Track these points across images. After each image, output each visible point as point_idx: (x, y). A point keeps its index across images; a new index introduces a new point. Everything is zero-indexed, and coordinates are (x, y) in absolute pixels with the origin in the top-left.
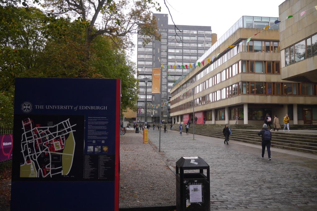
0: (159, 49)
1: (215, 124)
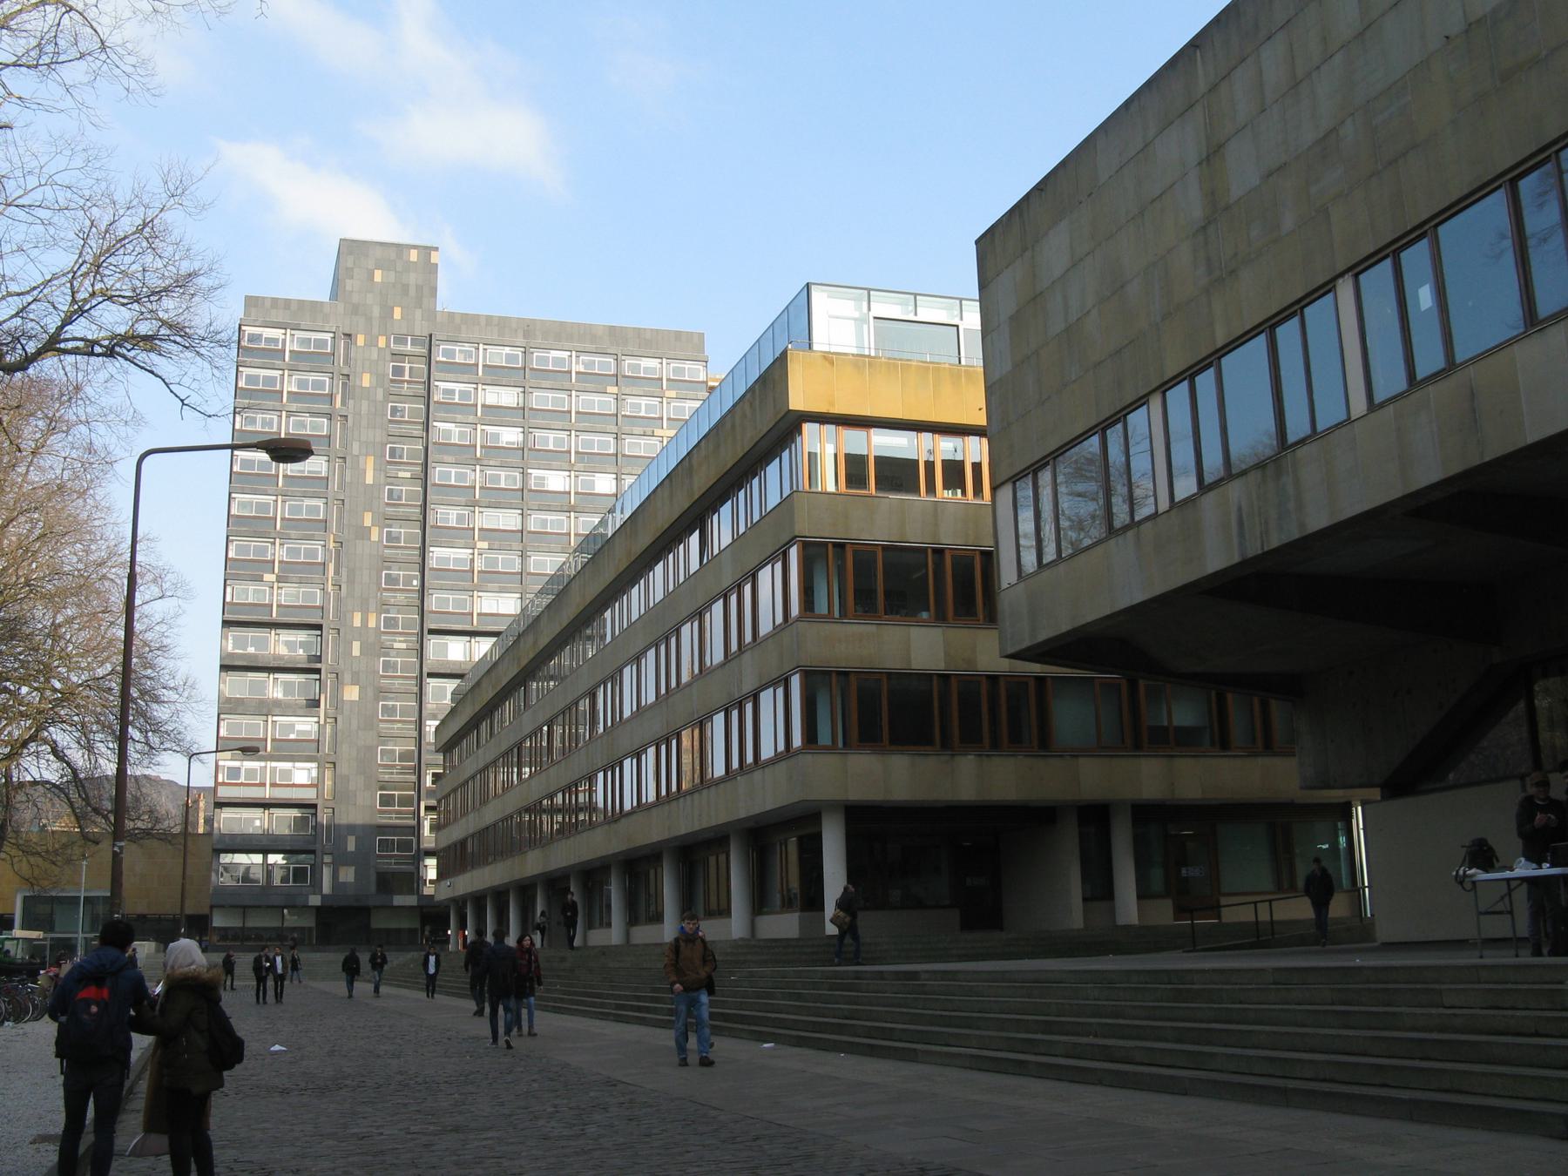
0: (370, 461)
1: (1257, 921)
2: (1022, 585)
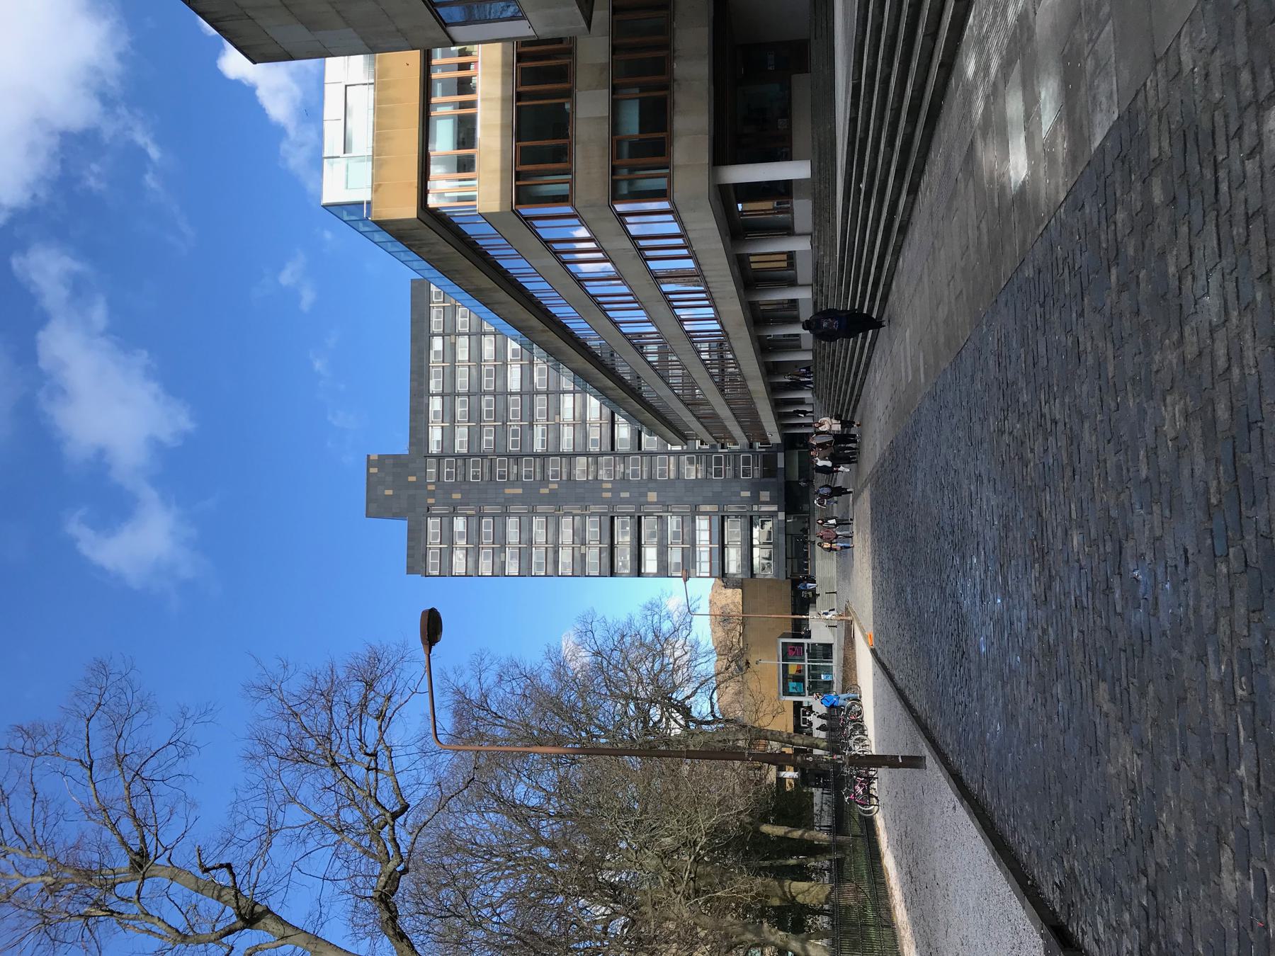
0: (508, 491)
1: (812, 350)
2: (529, 15)
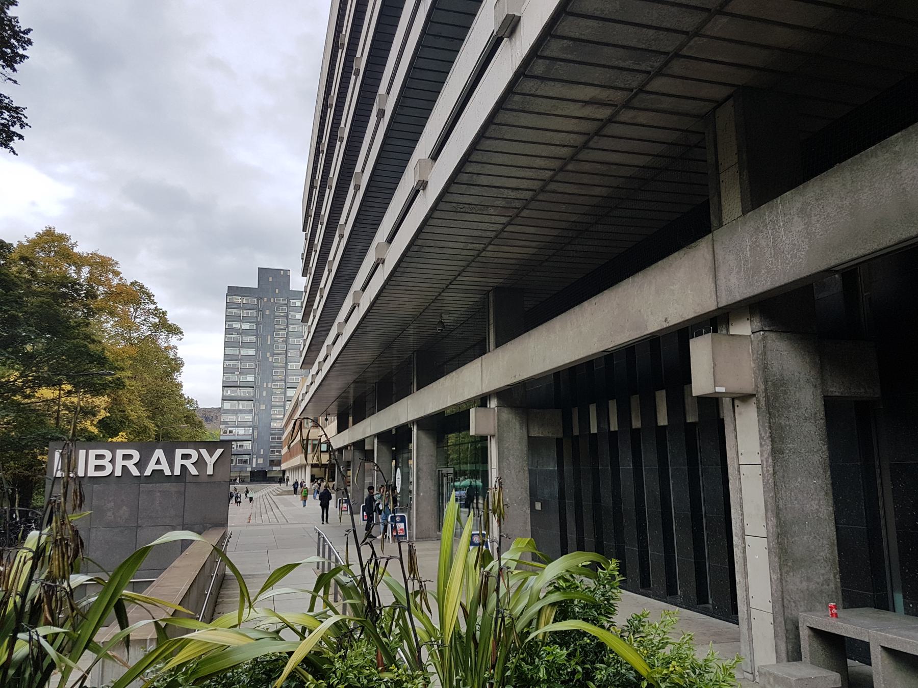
0: (269, 337)
